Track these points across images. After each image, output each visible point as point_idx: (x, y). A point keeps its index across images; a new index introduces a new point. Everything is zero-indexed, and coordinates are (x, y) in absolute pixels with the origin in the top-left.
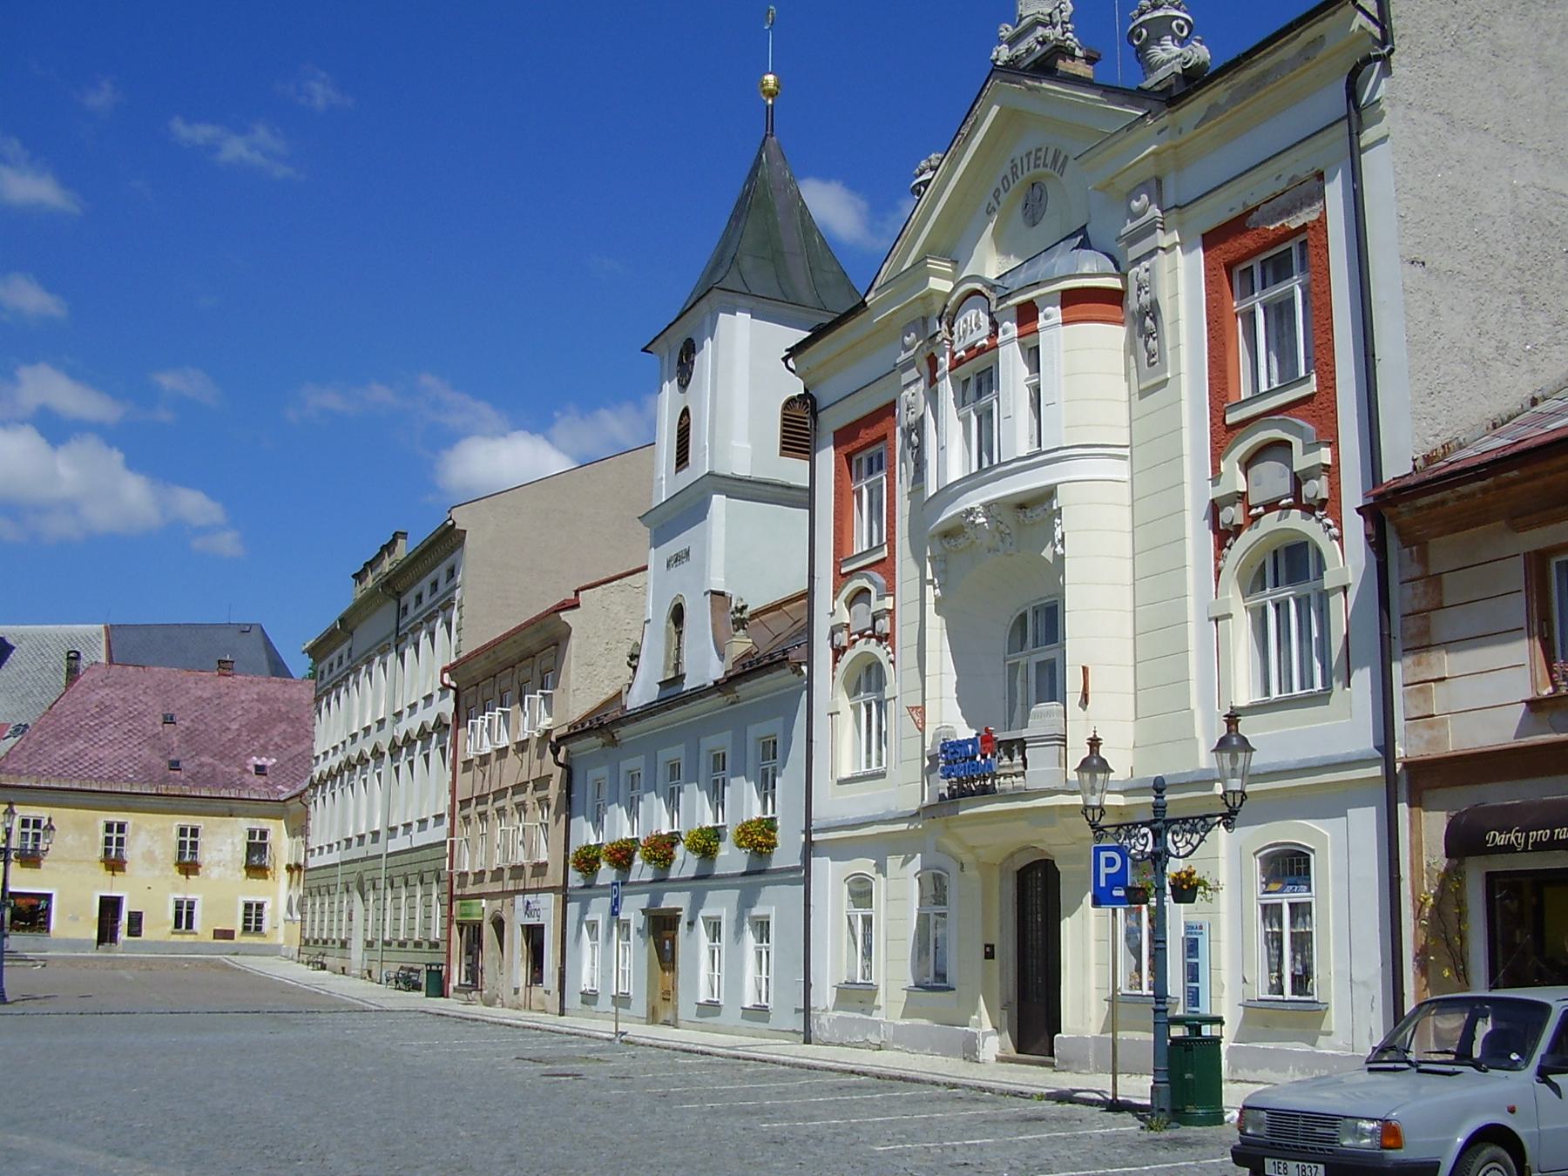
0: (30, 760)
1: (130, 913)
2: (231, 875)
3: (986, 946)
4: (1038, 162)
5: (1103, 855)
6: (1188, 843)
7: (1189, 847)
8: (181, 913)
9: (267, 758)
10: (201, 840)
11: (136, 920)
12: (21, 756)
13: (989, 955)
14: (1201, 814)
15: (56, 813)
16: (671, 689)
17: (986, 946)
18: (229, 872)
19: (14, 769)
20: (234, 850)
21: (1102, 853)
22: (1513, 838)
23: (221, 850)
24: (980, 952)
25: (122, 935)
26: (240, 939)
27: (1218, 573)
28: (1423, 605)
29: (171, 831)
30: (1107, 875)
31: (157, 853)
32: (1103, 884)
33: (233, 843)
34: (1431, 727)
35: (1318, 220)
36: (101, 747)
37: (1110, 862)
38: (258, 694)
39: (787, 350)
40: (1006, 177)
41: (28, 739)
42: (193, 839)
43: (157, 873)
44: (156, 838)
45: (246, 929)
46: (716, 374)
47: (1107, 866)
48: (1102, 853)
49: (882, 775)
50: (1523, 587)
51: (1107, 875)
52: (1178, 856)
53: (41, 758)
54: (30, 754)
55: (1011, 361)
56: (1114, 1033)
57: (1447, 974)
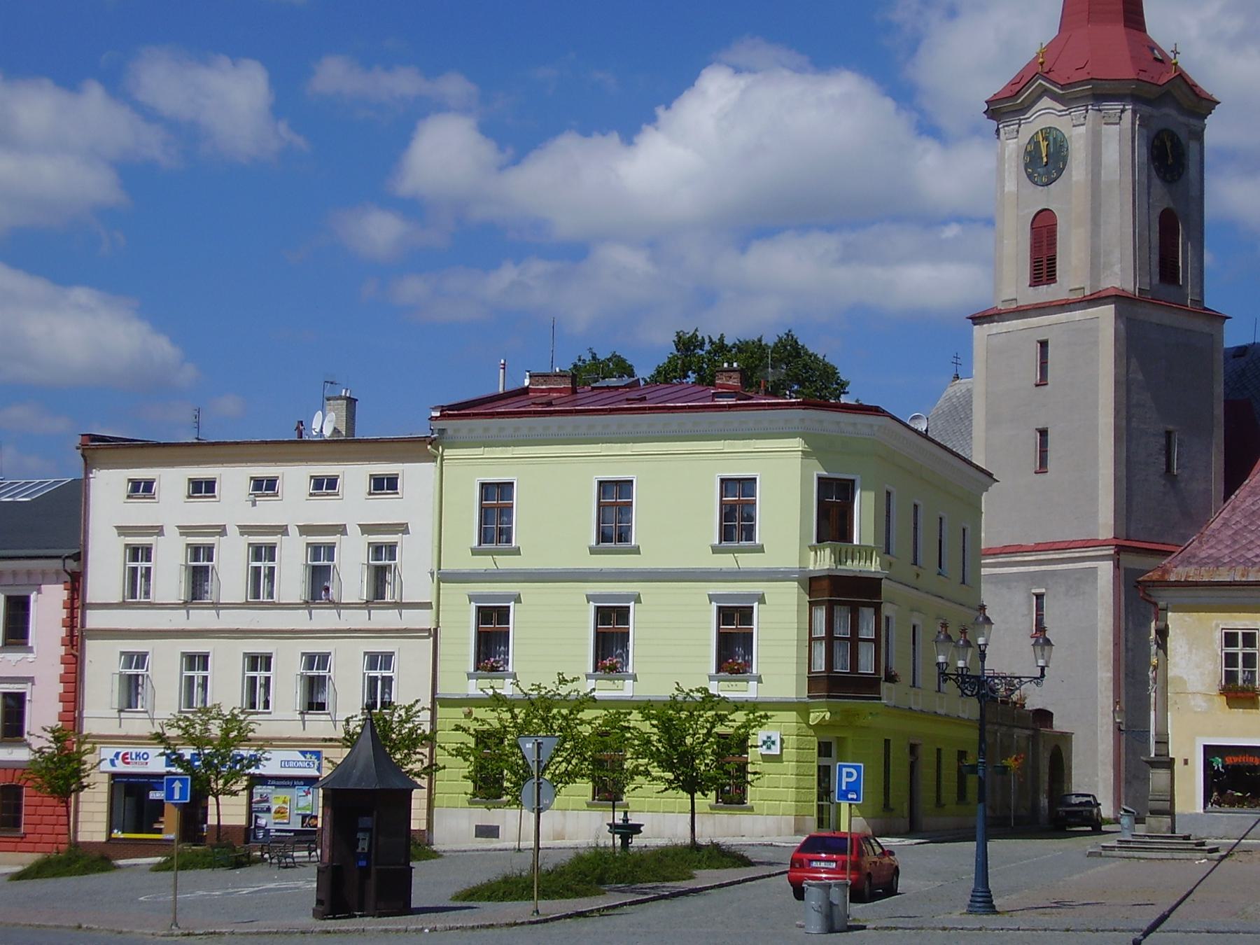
0: (1235, 542)
5: (845, 770)
12: (1221, 536)
15: (323, 749)
19: (1209, 557)
21: (844, 769)
25: (252, 840)
30: (847, 782)
32: (844, 788)
37: (849, 775)
41: (1234, 509)
46: (1132, 167)
47: (847, 777)
48: (844, 769)
51: (847, 782)
53: (1252, 537)
54: (1236, 533)
56: (175, 895)
57: (238, 873)
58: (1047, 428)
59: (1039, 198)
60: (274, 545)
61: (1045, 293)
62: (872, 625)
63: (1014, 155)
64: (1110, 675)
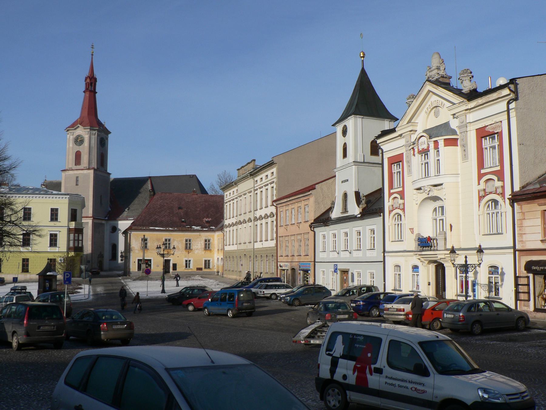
1: (173, 264)
2: (201, 252)
3: (428, 282)
4: (438, 102)
5: (335, 266)
6: (471, 269)
7: (472, 270)
8: (187, 263)
9: (209, 218)
10: (192, 242)
11: (175, 266)
13: (429, 284)
14: (474, 264)
16: (343, 215)
17: (428, 282)
18: (200, 252)
20: (201, 246)
22: (537, 268)
23: (198, 245)
24: (427, 284)
25: (171, 270)
26: (204, 270)
27: (479, 206)
28: (521, 218)
29: (183, 241)
31: (180, 247)
33: (201, 243)
34: (522, 243)
35: (501, 132)
36: (162, 217)
37: (67, 275)
38: (204, 199)
39: (375, 137)
40: (430, 105)
42: (187, 243)
43: (180, 253)
44: (179, 243)
45: (205, 267)
47: (67, 276)
49: (403, 241)
50: (540, 217)
52: (470, 271)
55: (432, 151)
58: (371, 155)
59: (77, 148)
60: (348, 270)
61: (78, 167)
62: (81, 238)
63: (72, 139)
64: (91, 243)
